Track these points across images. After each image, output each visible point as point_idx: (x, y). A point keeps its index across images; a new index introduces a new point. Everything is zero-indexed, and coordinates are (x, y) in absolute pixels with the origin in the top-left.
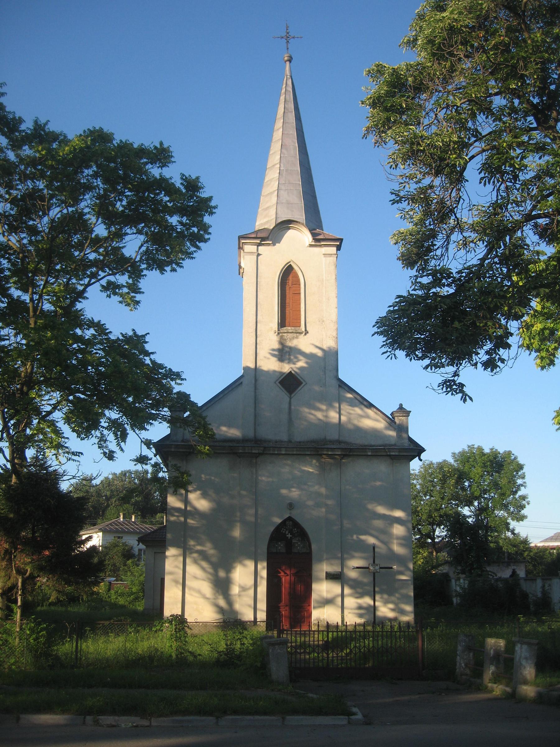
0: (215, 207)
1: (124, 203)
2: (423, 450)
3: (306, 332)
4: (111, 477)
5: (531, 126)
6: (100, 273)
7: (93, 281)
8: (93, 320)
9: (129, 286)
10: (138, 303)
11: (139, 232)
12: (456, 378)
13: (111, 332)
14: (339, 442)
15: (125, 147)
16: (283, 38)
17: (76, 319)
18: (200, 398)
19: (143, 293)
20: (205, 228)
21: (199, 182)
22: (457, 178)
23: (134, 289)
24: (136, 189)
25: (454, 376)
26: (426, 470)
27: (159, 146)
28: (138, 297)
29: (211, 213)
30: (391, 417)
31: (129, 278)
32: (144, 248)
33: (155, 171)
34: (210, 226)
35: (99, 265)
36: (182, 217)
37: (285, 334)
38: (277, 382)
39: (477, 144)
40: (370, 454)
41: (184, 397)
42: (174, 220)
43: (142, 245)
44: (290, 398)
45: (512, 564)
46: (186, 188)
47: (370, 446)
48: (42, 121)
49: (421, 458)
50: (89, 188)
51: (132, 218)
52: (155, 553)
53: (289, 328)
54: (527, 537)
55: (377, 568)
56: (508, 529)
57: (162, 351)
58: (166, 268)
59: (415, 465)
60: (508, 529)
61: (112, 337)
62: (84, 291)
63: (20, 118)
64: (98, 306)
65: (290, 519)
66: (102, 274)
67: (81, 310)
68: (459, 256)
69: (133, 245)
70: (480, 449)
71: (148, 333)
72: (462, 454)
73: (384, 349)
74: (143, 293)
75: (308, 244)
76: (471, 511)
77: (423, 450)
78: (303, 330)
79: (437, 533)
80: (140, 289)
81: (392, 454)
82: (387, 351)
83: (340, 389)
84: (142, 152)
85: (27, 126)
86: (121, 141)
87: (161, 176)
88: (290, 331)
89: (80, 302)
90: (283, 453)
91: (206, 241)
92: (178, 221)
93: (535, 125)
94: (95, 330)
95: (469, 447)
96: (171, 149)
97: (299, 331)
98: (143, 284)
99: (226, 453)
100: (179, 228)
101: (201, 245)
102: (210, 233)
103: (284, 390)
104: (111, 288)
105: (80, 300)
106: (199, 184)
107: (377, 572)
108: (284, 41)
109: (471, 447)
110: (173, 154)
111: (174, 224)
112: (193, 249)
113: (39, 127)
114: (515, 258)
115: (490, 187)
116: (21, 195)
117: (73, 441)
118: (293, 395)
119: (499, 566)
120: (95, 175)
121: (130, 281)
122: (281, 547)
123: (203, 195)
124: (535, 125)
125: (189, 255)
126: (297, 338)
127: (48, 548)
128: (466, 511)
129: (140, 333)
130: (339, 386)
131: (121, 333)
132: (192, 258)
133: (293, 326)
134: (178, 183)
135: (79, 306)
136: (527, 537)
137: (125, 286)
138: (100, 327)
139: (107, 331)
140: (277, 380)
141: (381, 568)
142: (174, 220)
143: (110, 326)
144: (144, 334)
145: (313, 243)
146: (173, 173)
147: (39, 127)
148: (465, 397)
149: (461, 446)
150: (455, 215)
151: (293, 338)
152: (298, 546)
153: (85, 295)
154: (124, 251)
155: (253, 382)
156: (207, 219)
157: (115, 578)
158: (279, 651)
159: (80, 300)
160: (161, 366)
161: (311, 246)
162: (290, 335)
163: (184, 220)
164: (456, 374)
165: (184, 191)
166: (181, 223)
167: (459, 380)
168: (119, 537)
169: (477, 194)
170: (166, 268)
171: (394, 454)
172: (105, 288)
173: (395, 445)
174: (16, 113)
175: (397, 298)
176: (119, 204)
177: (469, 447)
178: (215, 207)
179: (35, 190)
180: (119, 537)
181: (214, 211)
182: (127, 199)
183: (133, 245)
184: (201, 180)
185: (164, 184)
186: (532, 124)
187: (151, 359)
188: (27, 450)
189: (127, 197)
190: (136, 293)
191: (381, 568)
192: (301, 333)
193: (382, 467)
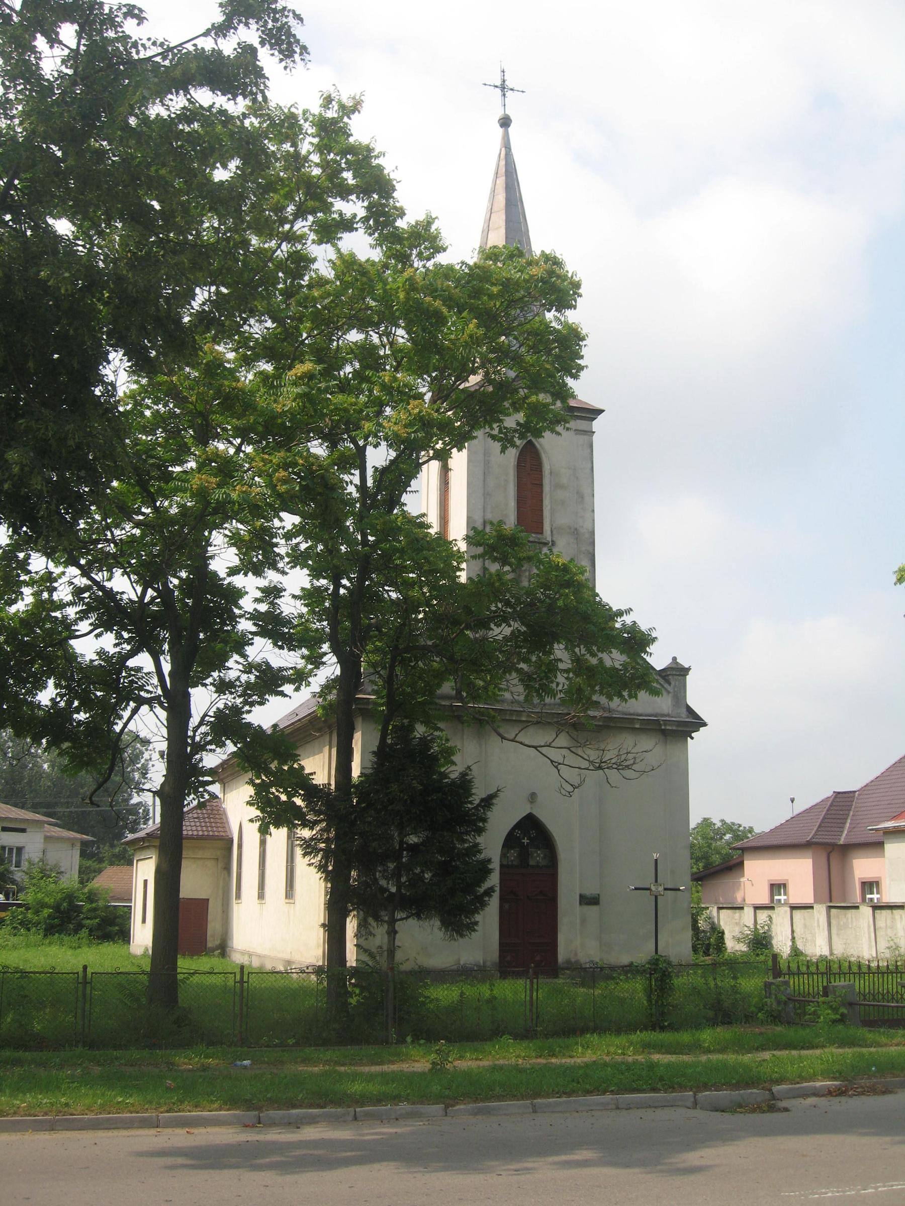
40: (637, 726)
55: (661, 889)
90: (524, 719)
107: (661, 895)
108: (498, 91)
122: (513, 854)
141: (665, 889)
148: (257, 588)
152: (538, 857)
173: (668, 715)
191: (665, 889)
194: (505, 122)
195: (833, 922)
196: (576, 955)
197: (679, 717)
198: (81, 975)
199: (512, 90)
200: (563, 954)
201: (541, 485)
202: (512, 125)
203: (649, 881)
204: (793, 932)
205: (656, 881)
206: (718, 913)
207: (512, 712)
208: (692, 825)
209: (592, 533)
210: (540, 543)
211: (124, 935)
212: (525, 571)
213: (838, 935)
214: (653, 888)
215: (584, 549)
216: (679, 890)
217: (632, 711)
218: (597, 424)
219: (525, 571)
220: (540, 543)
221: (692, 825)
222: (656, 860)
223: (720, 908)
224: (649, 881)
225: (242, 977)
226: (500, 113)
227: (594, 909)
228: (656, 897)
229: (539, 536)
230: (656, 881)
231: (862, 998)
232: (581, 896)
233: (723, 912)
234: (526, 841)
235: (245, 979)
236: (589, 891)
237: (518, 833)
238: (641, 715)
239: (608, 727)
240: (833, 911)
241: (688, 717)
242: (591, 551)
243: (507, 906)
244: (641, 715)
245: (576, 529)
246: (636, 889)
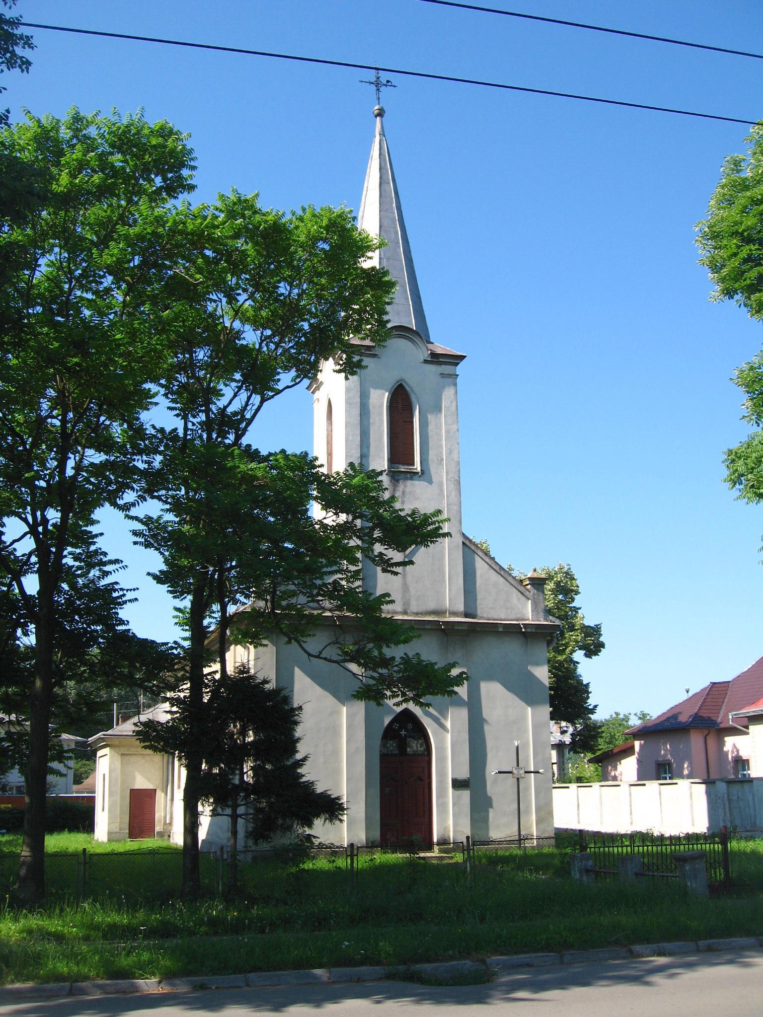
40: (501, 630)
52: (122, 754)
55: (522, 772)
75: (422, 360)
78: (419, 469)
108: (373, 87)
122: (392, 745)
131: (283, 451)
152: (415, 746)
161: (426, 362)
191: (526, 772)
198: (465, 844)
205: (518, 765)
208: (296, 669)
211: (89, 827)
214: (515, 771)
217: (496, 617)
218: (460, 369)
221: (296, 669)
228: (518, 779)
230: (518, 765)
231: (646, 868)
234: (403, 733)
237: (396, 726)
239: (474, 631)
243: (387, 790)
246: (500, 772)
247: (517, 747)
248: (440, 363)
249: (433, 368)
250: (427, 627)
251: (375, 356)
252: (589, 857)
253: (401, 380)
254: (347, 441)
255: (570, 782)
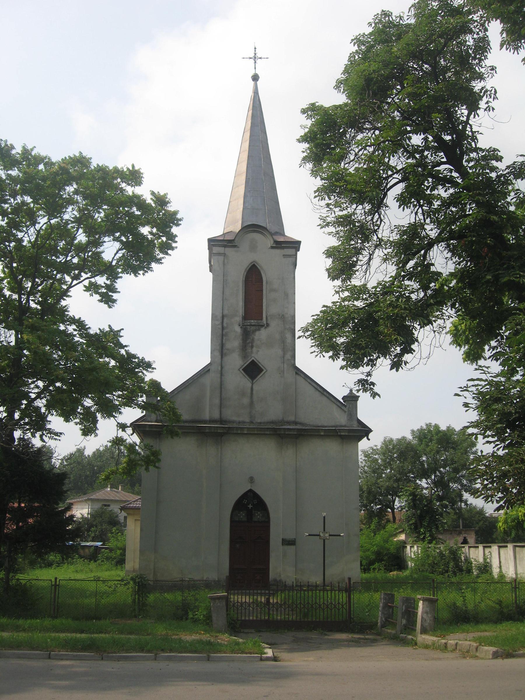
0: (180, 220)
1: (102, 215)
2: (370, 431)
3: (268, 325)
4: (101, 449)
5: (442, 160)
6: (83, 274)
7: (75, 282)
8: (74, 317)
9: (107, 287)
10: (114, 301)
11: (116, 239)
12: (369, 378)
13: (89, 328)
14: (296, 423)
15: (102, 170)
16: (251, 58)
17: (62, 315)
18: (169, 385)
19: (119, 292)
20: (172, 237)
21: (166, 198)
22: (378, 205)
23: (111, 288)
24: (112, 204)
25: (367, 376)
26: (387, 446)
27: (131, 169)
28: (115, 296)
29: (178, 225)
30: (342, 401)
31: (107, 279)
32: (120, 255)
33: (130, 190)
34: (176, 236)
35: (82, 267)
36: (153, 228)
37: (249, 327)
38: (241, 370)
39: (395, 176)
40: (322, 434)
41: (155, 385)
42: (145, 230)
43: (117, 252)
44: (252, 384)
45: (463, 532)
46: (155, 203)
47: (323, 427)
48: (29, 147)
49: (369, 437)
50: (70, 202)
51: (111, 228)
52: (136, 520)
53: (252, 321)
54: (483, 508)
55: (327, 535)
56: (461, 501)
57: (134, 343)
58: (139, 272)
59: (364, 445)
60: (461, 501)
61: (92, 332)
62: (67, 290)
63: (11, 145)
64: (80, 303)
65: (251, 491)
66: (84, 276)
67: (66, 306)
68: (377, 271)
69: (110, 250)
70: (437, 426)
71: (123, 329)
72: (421, 430)
73: (314, 349)
74: (119, 292)
76: (427, 483)
77: (370, 431)
78: (265, 323)
79: (396, 503)
80: (117, 289)
81: (342, 434)
82: (315, 351)
83: (297, 376)
84: (118, 172)
85: (18, 150)
86: (98, 165)
87: (133, 193)
88: (253, 324)
89: (64, 300)
90: (246, 432)
91: (172, 249)
92: (149, 232)
93: (445, 160)
94: (76, 325)
95: (427, 425)
96: (142, 171)
97: (262, 324)
98: (119, 284)
99: (194, 433)
100: (150, 237)
101: (170, 252)
102: (176, 242)
103: (246, 376)
104: (93, 288)
105: (65, 298)
106: (167, 200)
108: (252, 61)
109: (428, 425)
110: (143, 176)
111: (145, 234)
112: (161, 255)
113: (26, 152)
114: (425, 274)
115: (408, 211)
116: (11, 209)
117: (55, 422)
118: (254, 381)
119: (451, 534)
120: (76, 192)
121: (108, 282)
122: (242, 515)
123: (169, 209)
124: (445, 160)
125: (158, 261)
126: (259, 330)
127: (33, 517)
128: (424, 483)
129: (116, 328)
130: (296, 373)
132: (161, 263)
133: (256, 320)
134: (149, 199)
135: (63, 303)
136: (483, 508)
137: (103, 287)
138: (80, 324)
139: (87, 327)
140: (241, 368)
141: (330, 535)
142: (145, 230)
143: (89, 323)
144: (119, 329)
145: (274, 245)
146: (144, 191)
147: (26, 152)
149: (419, 424)
150: (377, 236)
151: (256, 330)
152: (258, 516)
153: (69, 294)
154: (103, 255)
155: (220, 369)
156: (175, 230)
157: (101, 543)
158: (219, 604)
159: (65, 298)
160: (134, 356)
161: (272, 247)
162: (253, 328)
163: (155, 230)
164: (369, 374)
165: (153, 205)
166: (151, 233)
167: (371, 379)
168: (105, 505)
169: (396, 216)
170: (139, 272)
171: (344, 434)
172: (87, 289)
173: (345, 426)
174: (8, 140)
175: (323, 307)
176: (97, 215)
177: (427, 425)
178: (180, 220)
179: (23, 203)
180: (105, 505)
181: (180, 222)
182: (105, 212)
183: (110, 250)
184: (169, 197)
185: (137, 201)
186: (443, 158)
187: (126, 350)
188: (15, 432)
189: (104, 210)
190: (113, 293)
191: (330, 535)
192: (263, 326)
193: (331, 448)
194: (255, 78)
195: (517, 556)
196: (280, 576)
197: (351, 427)
199: (260, 58)
200: (272, 575)
201: (262, 290)
202: (259, 80)
203: (318, 529)
204: (500, 562)
205: (324, 530)
206: (469, 550)
207: (237, 428)
209: (294, 317)
210: (258, 325)
212: (249, 343)
213: (520, 564)
214: (322, 535)
215: (288, 327)
216: (340, 536)
217: (320, 425)
219: (249, 343)
220: (258, 325)
222: (324, 517)
223: (470, 547)
224: (318, 529)
225: (516, 585)
226: (252, 73)
227: (293, 547)
228: (324, 540)
229: (260, 321)
230: (324, 530)
232: (283, 540)
233: (472, 549)
234: (250, 506)
235: (517, 586)
236: (290, 536)
238: (326, 427)
240: (517, 549)
241: (358, 427)
242: (293, 327)
244: (326, 427)
245: (283, 315)
247: (324, 517)
248: (283, 248)
249: (278, 252)
250: (266, 433)
251: (235, 246)
252: (265, 594)
253: (254, 261)
254: (294, 303)
255: (507, 543)
